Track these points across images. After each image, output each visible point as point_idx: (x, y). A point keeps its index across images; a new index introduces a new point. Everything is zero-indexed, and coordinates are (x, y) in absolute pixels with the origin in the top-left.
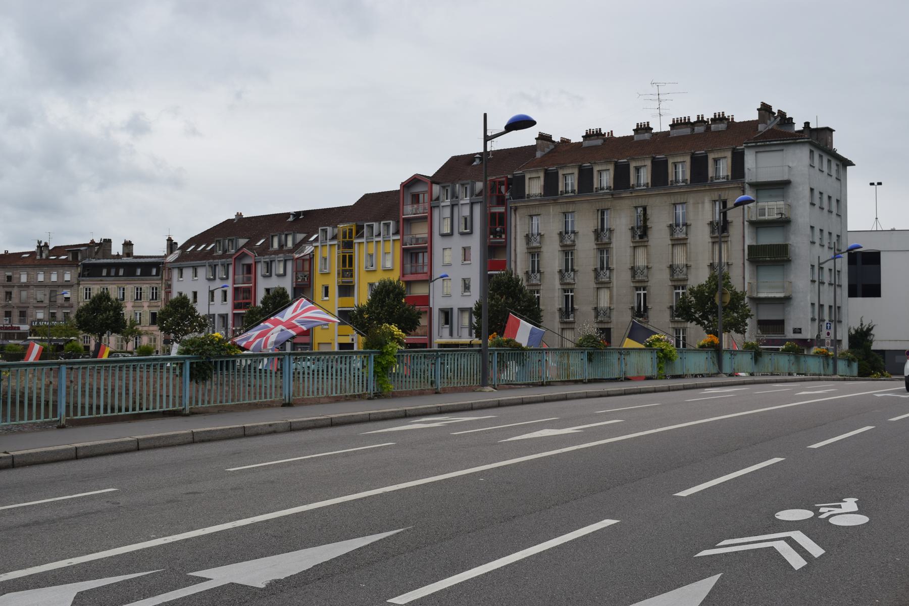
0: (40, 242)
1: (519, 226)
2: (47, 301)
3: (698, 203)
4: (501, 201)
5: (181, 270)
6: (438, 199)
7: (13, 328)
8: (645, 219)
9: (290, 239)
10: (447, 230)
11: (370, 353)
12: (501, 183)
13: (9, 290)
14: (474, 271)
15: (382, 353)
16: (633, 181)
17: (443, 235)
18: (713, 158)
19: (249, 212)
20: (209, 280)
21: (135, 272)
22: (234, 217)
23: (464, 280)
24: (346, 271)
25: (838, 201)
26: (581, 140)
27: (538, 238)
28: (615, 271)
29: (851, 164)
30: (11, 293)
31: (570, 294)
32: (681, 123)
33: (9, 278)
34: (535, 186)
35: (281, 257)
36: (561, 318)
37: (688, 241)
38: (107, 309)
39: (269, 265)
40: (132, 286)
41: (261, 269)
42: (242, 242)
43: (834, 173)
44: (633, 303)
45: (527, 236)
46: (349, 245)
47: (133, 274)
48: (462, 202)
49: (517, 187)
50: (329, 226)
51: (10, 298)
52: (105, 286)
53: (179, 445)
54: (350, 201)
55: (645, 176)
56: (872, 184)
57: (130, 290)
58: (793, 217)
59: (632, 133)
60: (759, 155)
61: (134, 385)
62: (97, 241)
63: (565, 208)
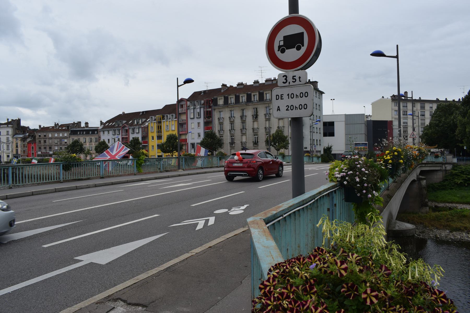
0: (55, 123)
1: (216, 115)
2: (59, 143)
4: (210, 107)
5: (104, 132)
6: (189, 106)
7: (47, 153)
8: (257, 112)
9: (140, 120)
10: (192, 117)
11: (134, 160)
12: (210, 101)
13: (45, 140)
14: (201, 130)
15: (139, 160)
16: (253, 99)
17: (191, 119)
19: (128, 111)
20: (113, 135)
21: (89, 133)
22: (122, 113)
23: (198, 133)
24: (160, 131)
25: (319, 105)
26: (236, 86)
27: (222, 119)
29: (323, 93)
30: (46, 141)
31: (233, 137)
33: (45, 136)
34: (221, 102)
35: (137, 127)
36: (230, 145)
38: (78, 146)
39: (133, 130)
40: (88, 137)
41: (131, 131)
42: (124, 122)
43: (318, 96)
44: (253, 140)
45: (219, 118)
46: (160, 122)
47: (89, 133)
48: (197, 107)
49: (215, 102)
50: (168, 114)
51: (46, 143)
52: (79, 138)
53: (50, 193)
54: (161, 107)
55: (257, 98)
56: (331, 100)
57: (88, 139)
59: (253, 84)
61: (87, 171)
62: (76, 122)
63: (231, 109)
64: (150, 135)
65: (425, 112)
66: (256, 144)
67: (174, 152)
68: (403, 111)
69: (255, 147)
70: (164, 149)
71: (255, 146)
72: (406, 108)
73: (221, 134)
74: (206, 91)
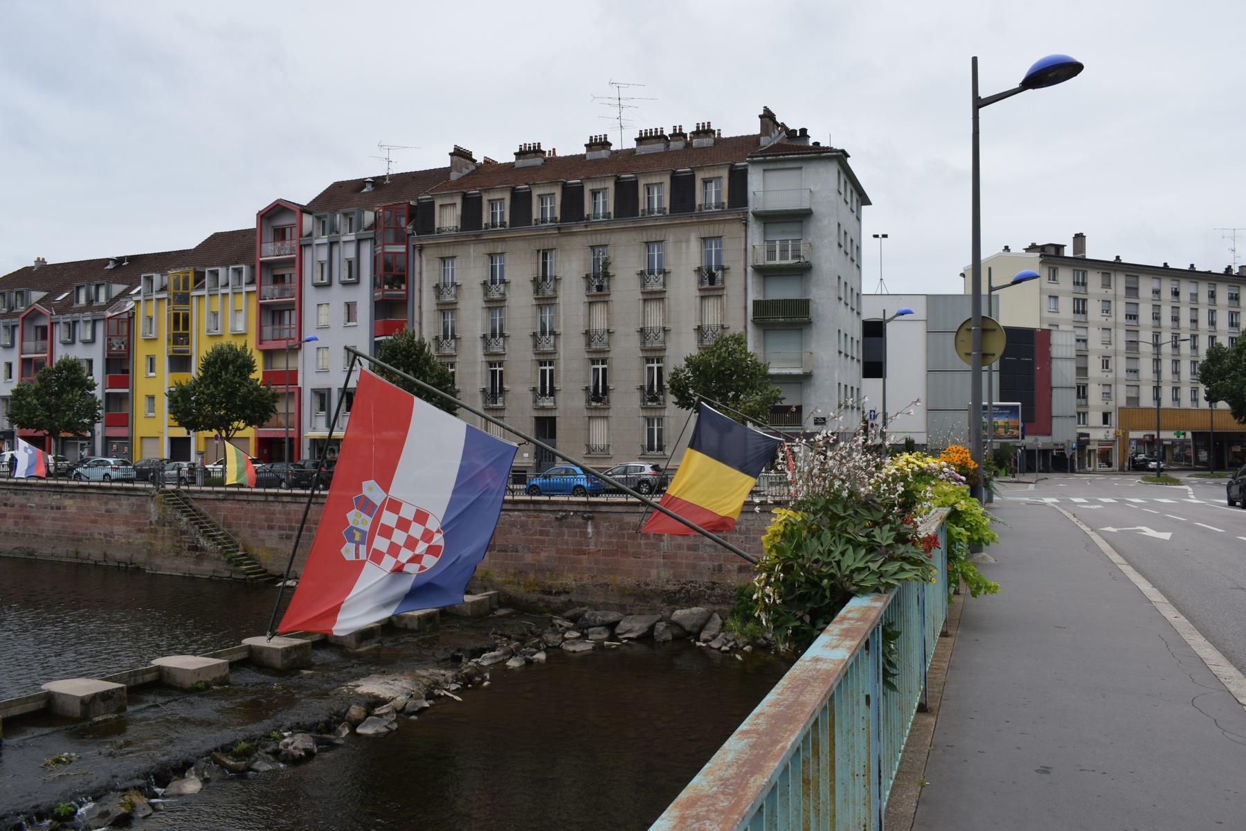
1: (426, 273)
3: (681, 242)
9: (102, 291)
14: (361, 337)
16: (588, 210)
17: (317, 286)
18: (703, 179)
22: (33, 264)
28: (562, 338)
29: (869, 203)
31: (498, 369)
32: (651, 137)
34: (448, 218)
35: (88, 316)
36: (485, 402)
37: (667, 295)
39: (72, 327)
41: (60, 333)
42: (36, 296)
44: (588, 382)
45: (437, 286)
46: (184, 299)
49: (422, 217)
50: (221, 265)
56: (876, 236)
58: (814, 262)
60: (770, 175)
63: (490, 248)
64: (141, 352)
65: (1137, 304)
66: (598, 400)
67: (236, 424)
68: (1074, 299)
69: (594, 414)
70: (187, 413)
71: (596, 408)
72: (1082, 289)
73: (448, 351)
74: (383, 178)
